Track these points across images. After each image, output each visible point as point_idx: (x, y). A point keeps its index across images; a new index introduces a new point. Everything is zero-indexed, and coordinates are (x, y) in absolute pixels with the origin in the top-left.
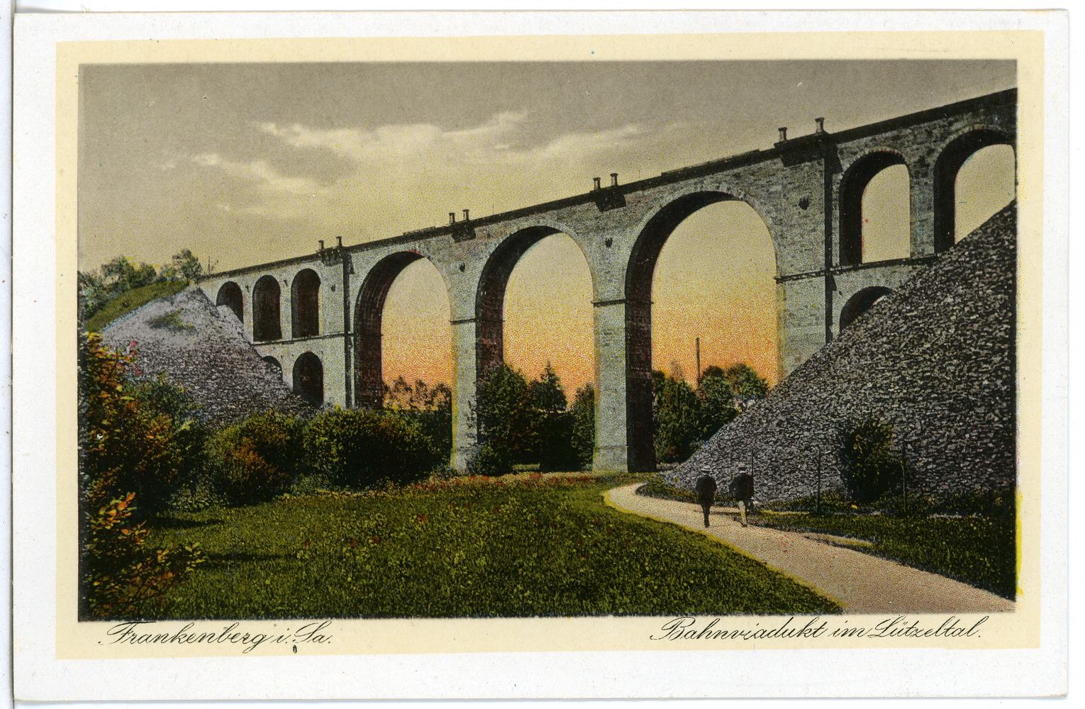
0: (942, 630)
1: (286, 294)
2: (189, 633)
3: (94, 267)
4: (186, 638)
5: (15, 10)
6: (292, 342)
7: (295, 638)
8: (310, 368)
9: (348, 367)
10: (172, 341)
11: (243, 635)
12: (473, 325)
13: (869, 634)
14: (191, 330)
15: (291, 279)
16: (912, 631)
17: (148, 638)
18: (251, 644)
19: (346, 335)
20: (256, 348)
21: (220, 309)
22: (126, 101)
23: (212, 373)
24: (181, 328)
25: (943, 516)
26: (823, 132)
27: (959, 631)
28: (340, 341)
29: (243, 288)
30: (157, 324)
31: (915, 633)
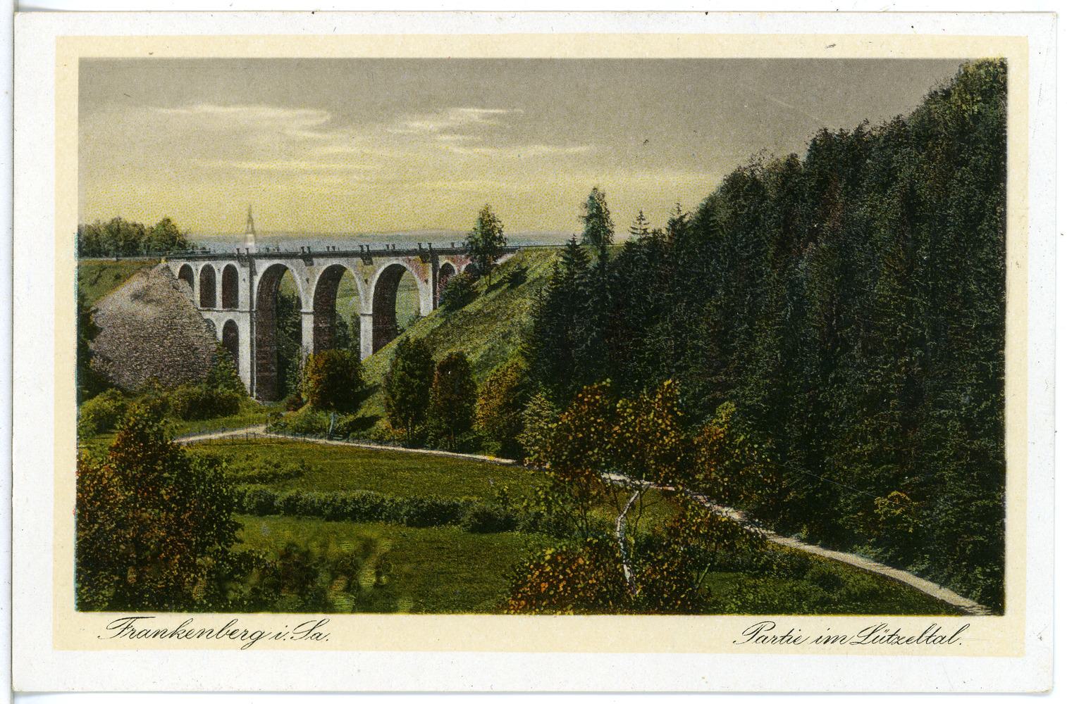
0: (924, 638)
1: (219, 278)
2: (188, 628)
3: (84, 223)
4: (185, 634)
5: (17, 9)
6: (222, 311)
7: (293, 635)
8: (231, 328)
11: (242, 631)
12: (302, 310)
13: (851, 641)
16: (895, 638)
17: (146, 633)
18: (250, 641)
19: (251, 312)
20: (202, 312)
23: (168, 334)
25: (903, 507)
27: (940, 639)
29: (194, 270)
31: (896, 640)
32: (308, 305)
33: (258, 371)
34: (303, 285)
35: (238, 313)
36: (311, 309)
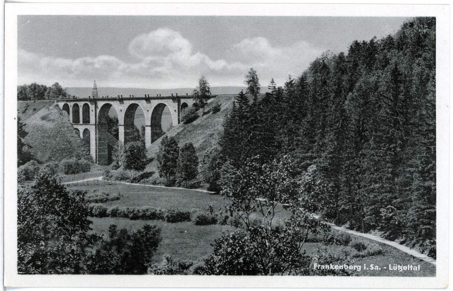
5: (6, 2)
6: (82, 125)
8: (86, 131)
9: (96, 134)
10: (49, 125)
14: (53, 121)
15: (82, 106)
21: (63, 111)
22: (39, 33)
24: (50, 120)
26: (150, 126)
28: (94, 127)
29: (70, 106)
30: (43, 118)
32: (121, 121)
33: (99, 146)
34: (119, 110)
35: (90, 126)
36: (123, 124)
